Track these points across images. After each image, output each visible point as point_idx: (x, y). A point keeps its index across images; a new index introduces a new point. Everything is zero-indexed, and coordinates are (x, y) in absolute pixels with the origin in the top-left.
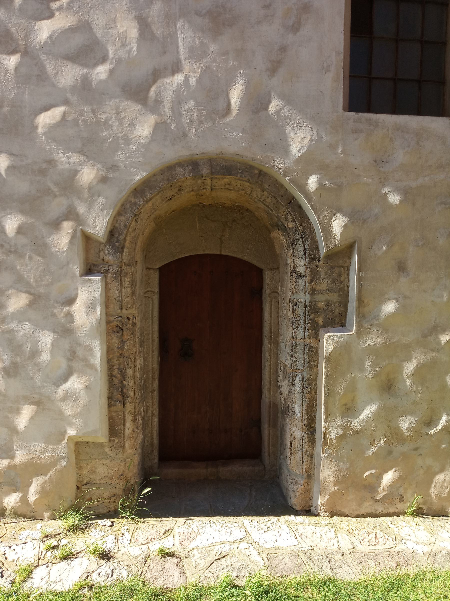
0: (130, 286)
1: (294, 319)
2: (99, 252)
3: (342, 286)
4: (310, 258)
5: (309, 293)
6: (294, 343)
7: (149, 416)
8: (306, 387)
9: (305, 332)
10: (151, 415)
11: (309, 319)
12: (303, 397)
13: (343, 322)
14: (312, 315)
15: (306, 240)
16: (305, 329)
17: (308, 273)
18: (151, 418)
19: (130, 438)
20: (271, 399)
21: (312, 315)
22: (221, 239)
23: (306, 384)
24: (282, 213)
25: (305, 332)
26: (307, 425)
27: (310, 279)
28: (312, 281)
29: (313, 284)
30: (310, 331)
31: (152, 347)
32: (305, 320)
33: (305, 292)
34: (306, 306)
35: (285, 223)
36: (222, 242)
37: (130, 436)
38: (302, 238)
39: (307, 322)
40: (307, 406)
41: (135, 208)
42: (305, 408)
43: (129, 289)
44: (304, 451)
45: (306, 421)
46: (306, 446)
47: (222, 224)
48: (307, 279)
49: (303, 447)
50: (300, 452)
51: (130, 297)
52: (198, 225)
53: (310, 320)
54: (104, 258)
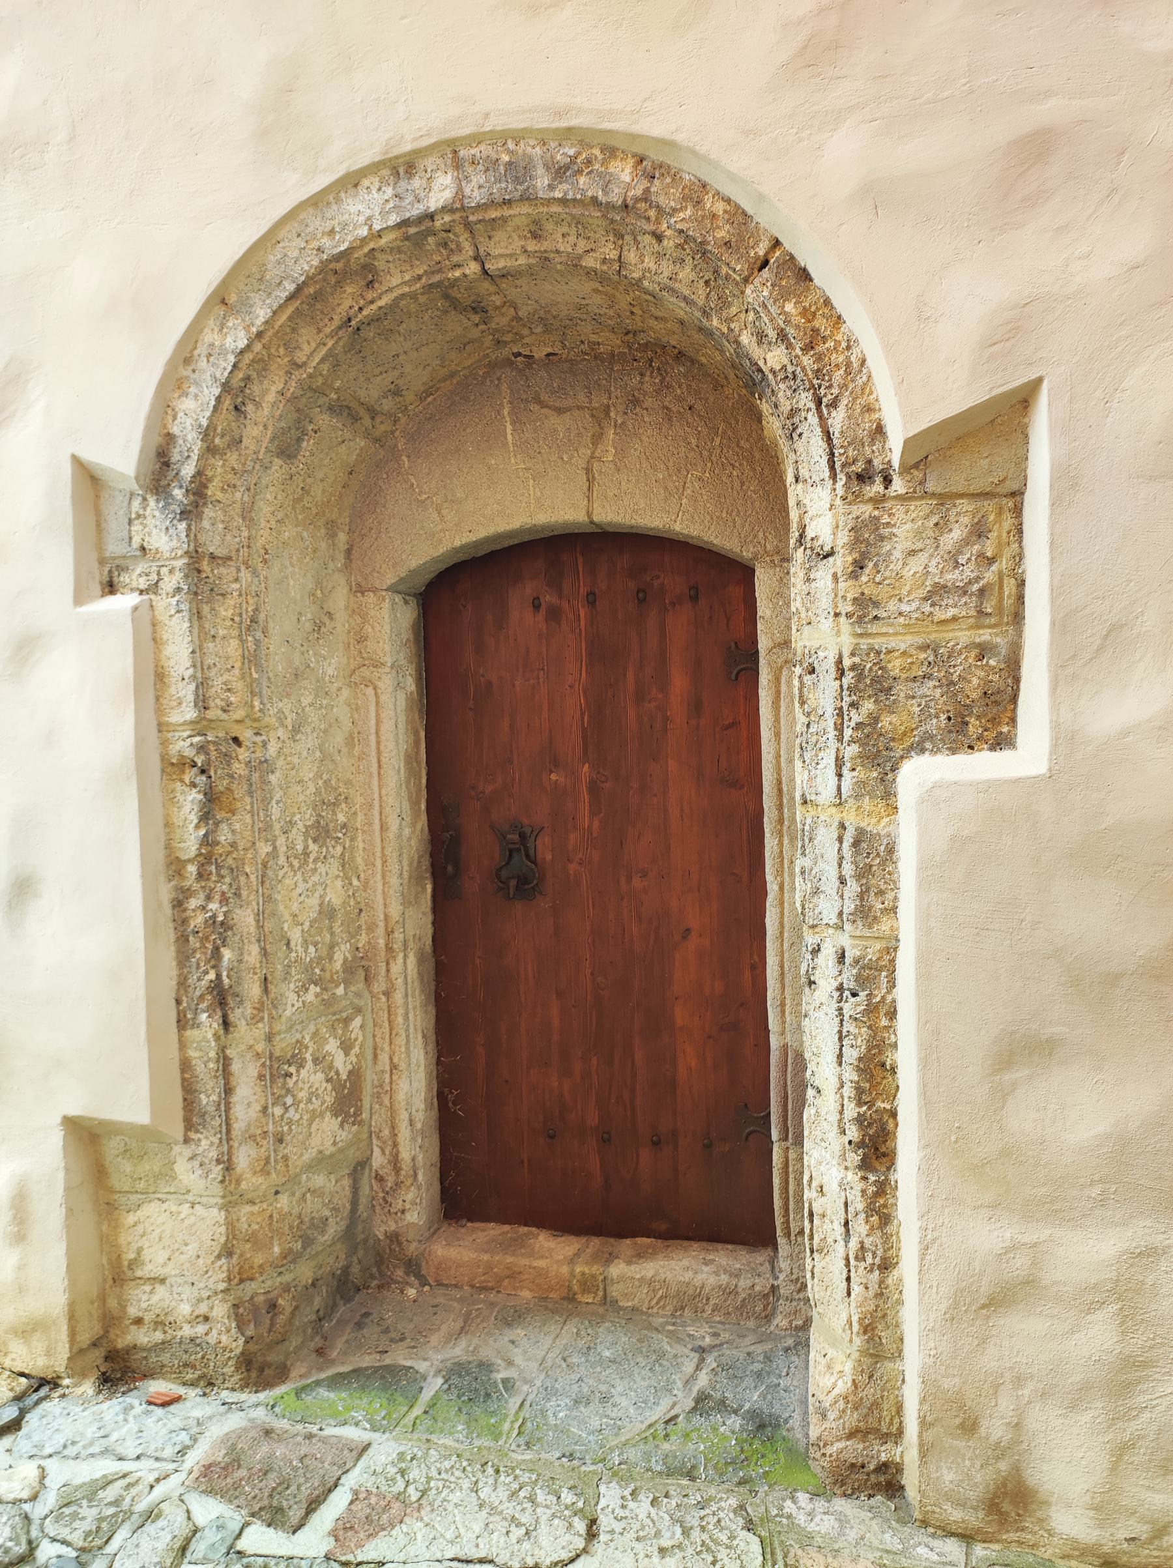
0: (235, 633)
1: (808, 726)
2: (130, 522)
3: (990, 575)
4: (848, 477)
5: (849, 616)
6: (809, 821)
7: (383, 1071)
8: (854, 995)
9: (840, 775)
10: (388, 1068)
11: (853, 724)
12: (840, 1032)
13: (1005, 729)
14: (868, 706)
15: (834, 404)
16: (839, 763)
17: (843, 538)
18: (387, 1076)
19: (252, 1137)
20: (788, 1039)
21: (868, 706)
22: (588, 470)
23: (848, 981)
24: (743, 315)
25: (840, 775)
26: (861, 1145)
27: (850, 559)
28: (859, 566)
29: (864, 579)
30: (860, 773)
31: (383, 848)
32: (839, 728)
33: (837, 615)
34: (841, 673)
35: (756, 352)
36: (590, 481)
37: (253, 1131)
38: (819, 403)
39: (848, 733)
40: (858, 1069)
41: (224, 364)
42: (850, 1075)
43: (234, 643)
44: (854, 1244)
45: (854, 1128)
46: (860, 1227)
47: (592, 416)
48: (841, 562)
49: (848, 1231)
50: (840, 1248)
51: (236, 671)
52: (509, 431)
53: (859, 726)
54: (145, 544)
